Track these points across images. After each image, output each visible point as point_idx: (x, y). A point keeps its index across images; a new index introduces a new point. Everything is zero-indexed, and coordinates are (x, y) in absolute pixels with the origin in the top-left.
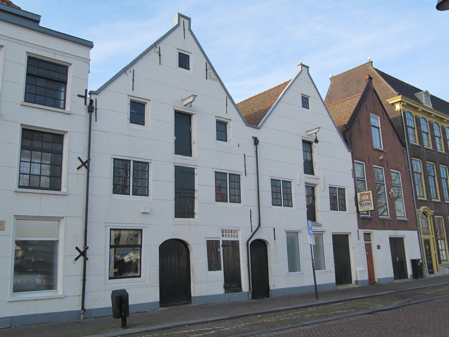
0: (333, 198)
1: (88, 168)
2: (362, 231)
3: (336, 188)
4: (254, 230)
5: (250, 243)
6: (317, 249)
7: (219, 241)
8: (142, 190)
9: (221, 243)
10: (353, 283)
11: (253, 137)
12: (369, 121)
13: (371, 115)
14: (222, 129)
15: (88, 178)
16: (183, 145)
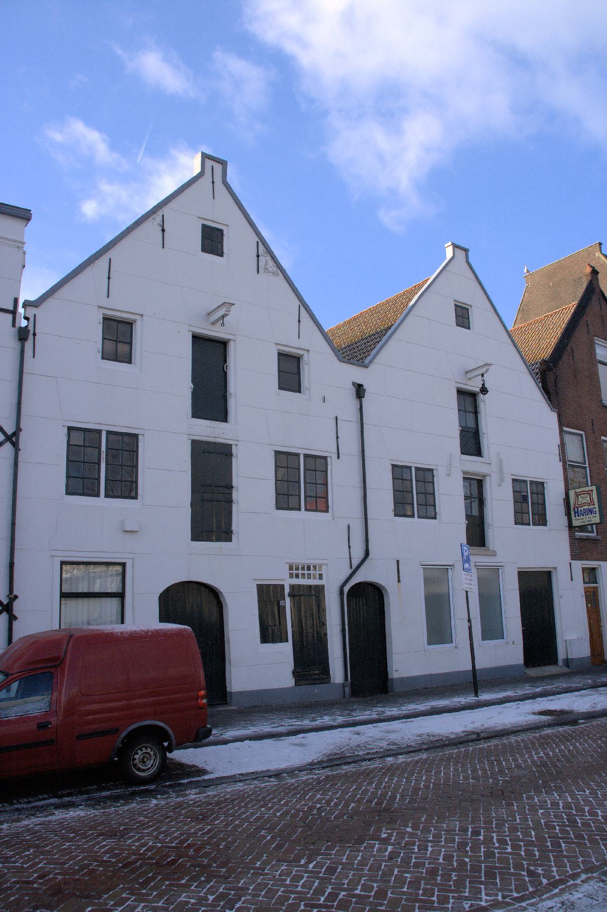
0: (520, 499)
1: (15, 445)
2: (578, 565)
3: (525, 482)
4: (355, 563)
5: (346, 589)
6: (490, 601)
7: (283, 585)
8: (125, 485)
9: (287, 590)
10: (560, 663)
11: (354, 384)
12: (593, 353)
13: (598, 341)
14: (290, 370)
15: (16, 464)
16: (210, 398)
